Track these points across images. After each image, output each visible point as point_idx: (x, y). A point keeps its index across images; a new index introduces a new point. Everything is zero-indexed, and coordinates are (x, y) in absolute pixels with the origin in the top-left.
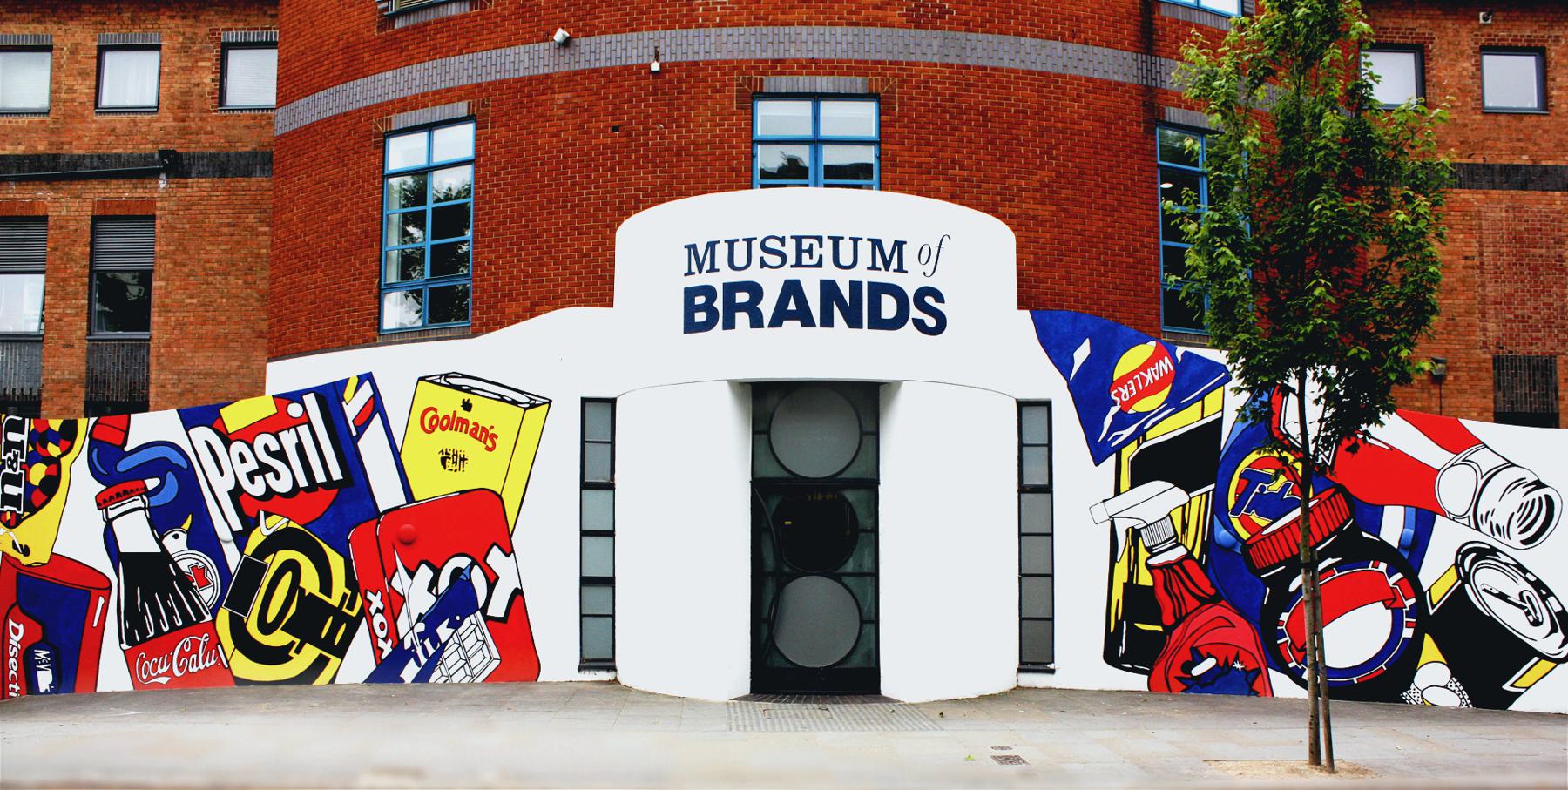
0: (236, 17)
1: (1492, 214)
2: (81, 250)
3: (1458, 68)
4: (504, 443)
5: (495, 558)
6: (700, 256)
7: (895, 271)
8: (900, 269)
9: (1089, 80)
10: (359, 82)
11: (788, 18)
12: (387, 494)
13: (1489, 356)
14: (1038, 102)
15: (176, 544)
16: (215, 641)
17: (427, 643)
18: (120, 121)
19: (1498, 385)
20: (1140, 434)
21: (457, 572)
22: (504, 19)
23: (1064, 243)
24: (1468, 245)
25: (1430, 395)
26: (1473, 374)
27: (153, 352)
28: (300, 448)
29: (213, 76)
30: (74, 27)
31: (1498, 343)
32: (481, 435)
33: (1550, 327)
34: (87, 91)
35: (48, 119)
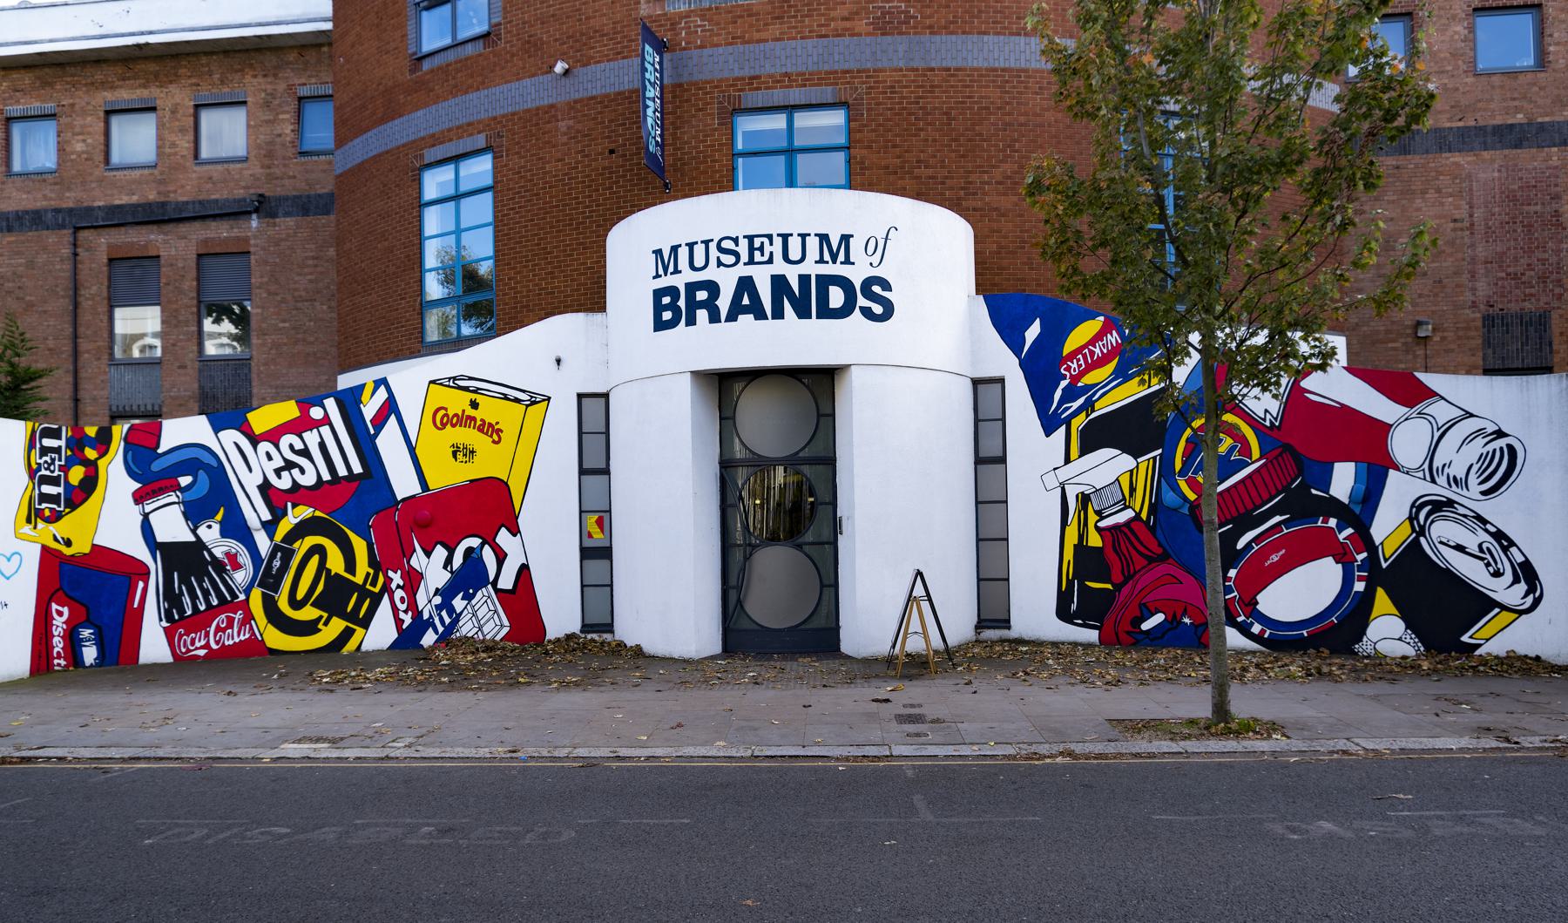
0: (309, 73)
1: (1485, 176)
2: (189, 284)
3: (1449, 33)
4: (508, 436)
5: (503, 538)
6: (665, 260)
7: (842, 263)
8: (847, 261)
10: (396, 122)
11: (763, 35)
12: (404, 484)
13: (1478, 315)
14: (1001, 98)
15: (210, 534)
16: (249, 617)
17: (444, 613)
18: (216, 170)
19: (1487, 343)
20: (1089, 406)
21: (469, 551)
22: (513, 55)
23: (1027, 231)
24: (1458, 208)
25: (1415, 357)
26: (1461, 333)
27: (254, 369)
28: (323, 446)
29: (292, 127)
30: (173, 88)
31: (1488, 302)
32: (488, 430)
33: (1546, 282)
34: (187, 145)
35: (156, 172)
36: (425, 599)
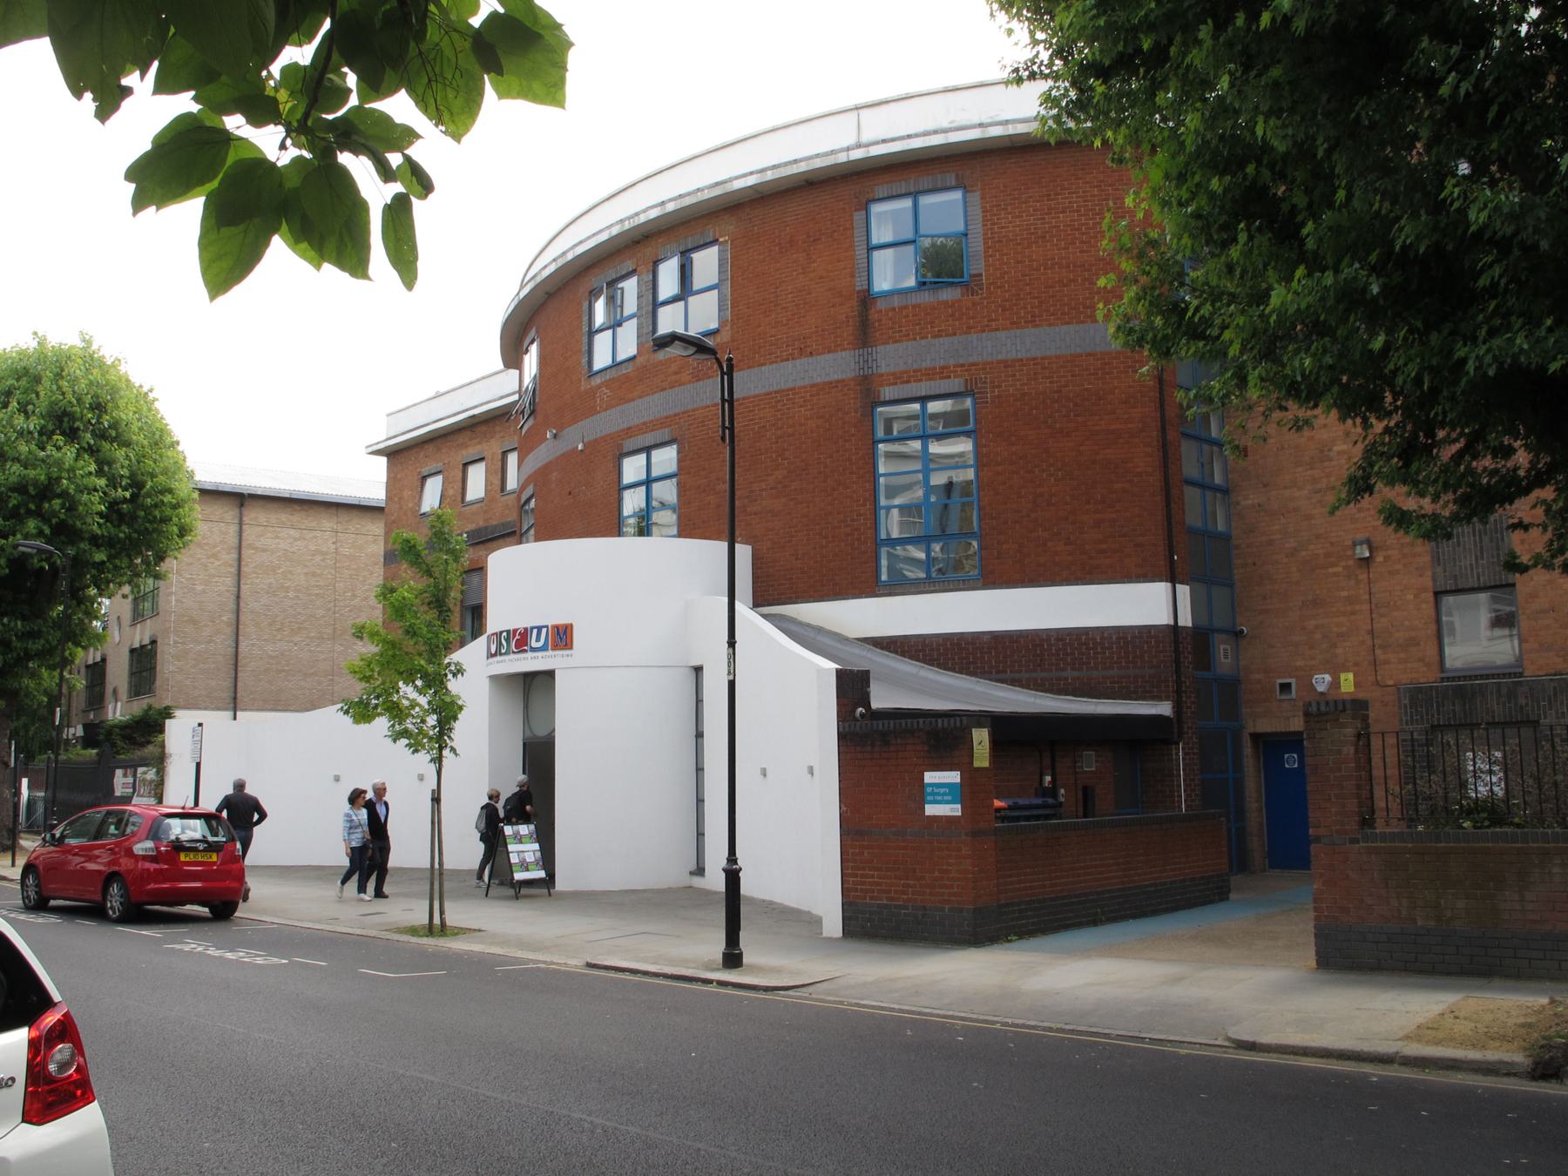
9: (813, 386)
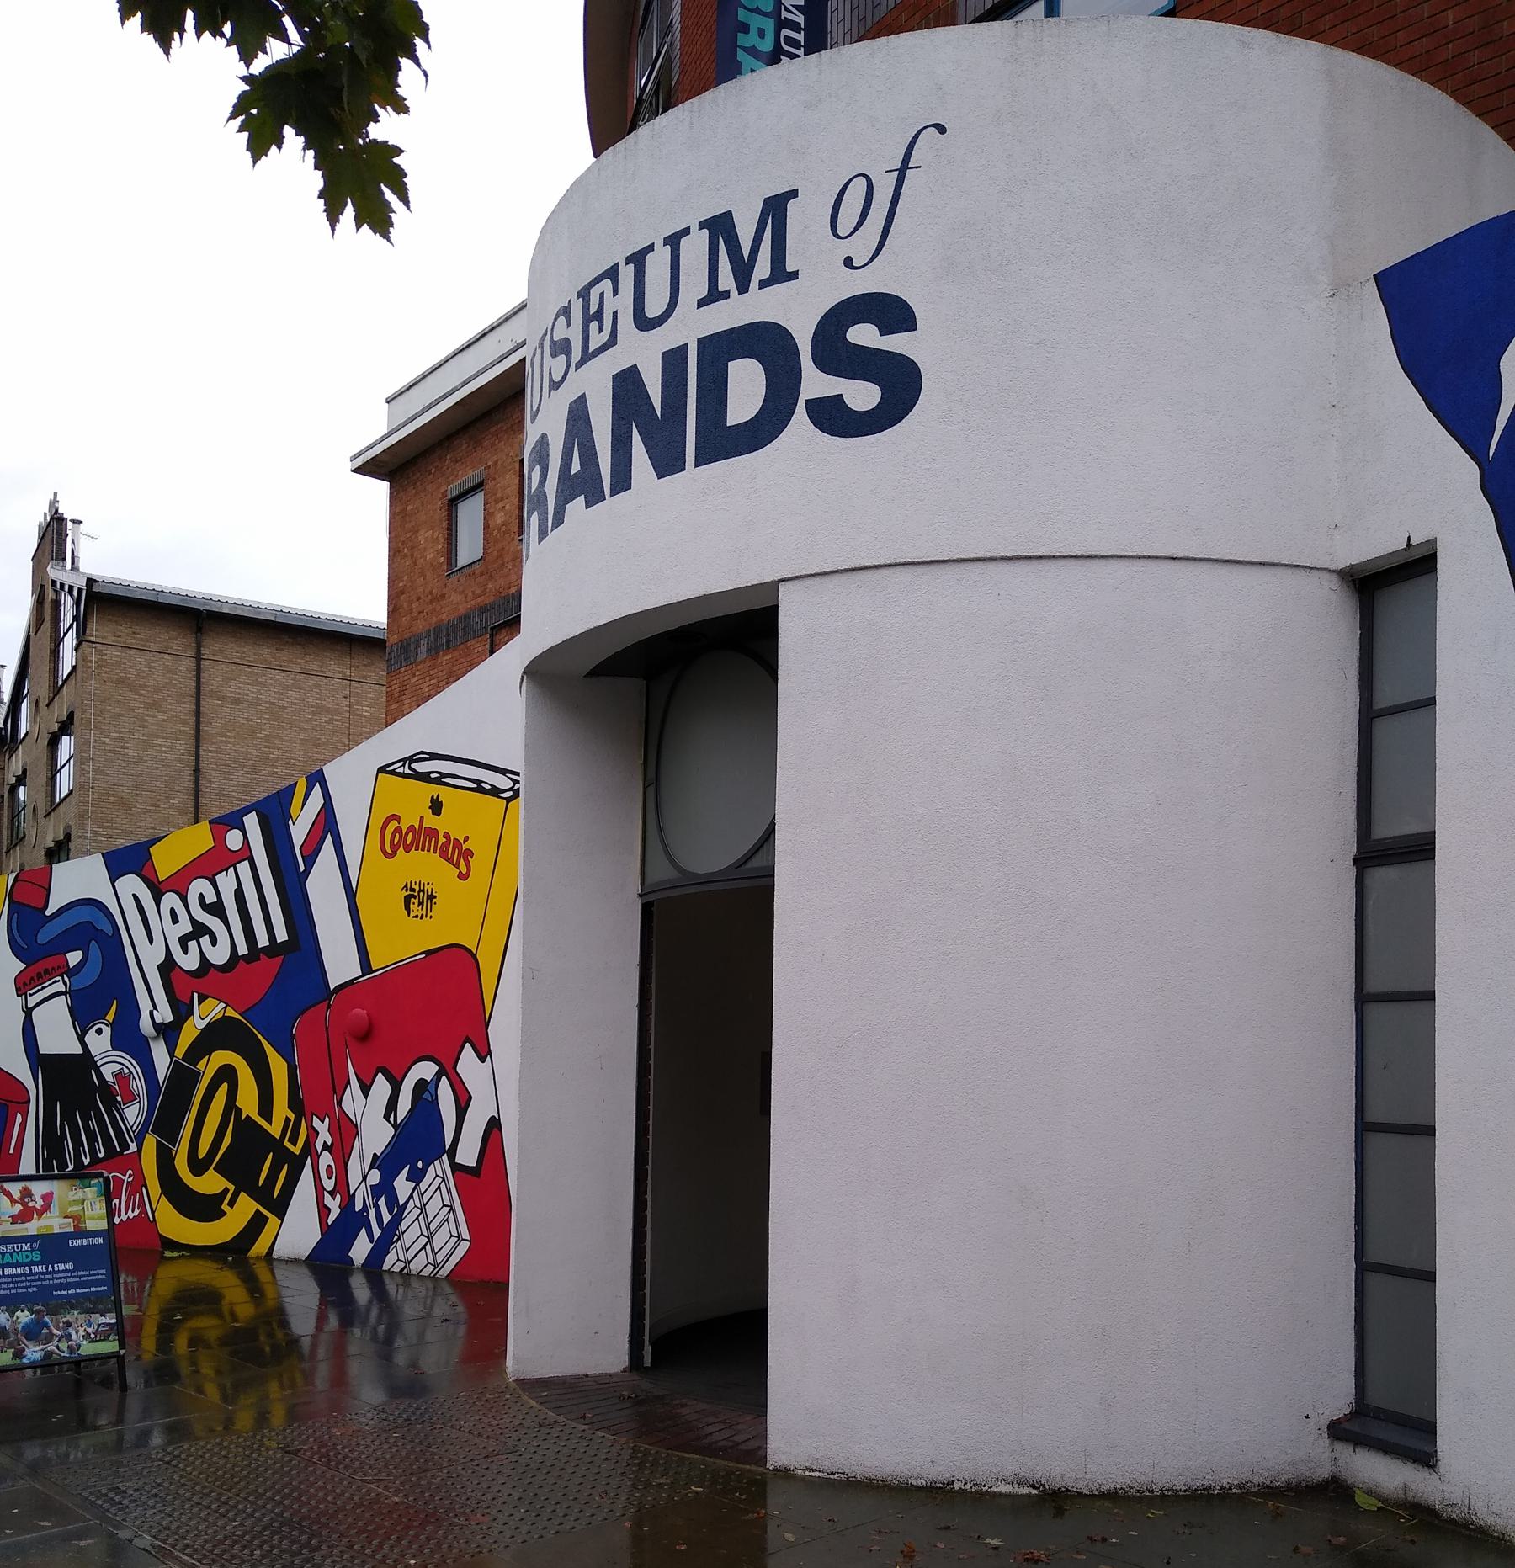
4: (481, 864)
8: (781, 274)
12: (340, 965)
15: (99, 1042)
16: (140, 1183)
17: (382, 1202)
21: (421, 1085)
28: (239, 895)
36: (361, 1176)
